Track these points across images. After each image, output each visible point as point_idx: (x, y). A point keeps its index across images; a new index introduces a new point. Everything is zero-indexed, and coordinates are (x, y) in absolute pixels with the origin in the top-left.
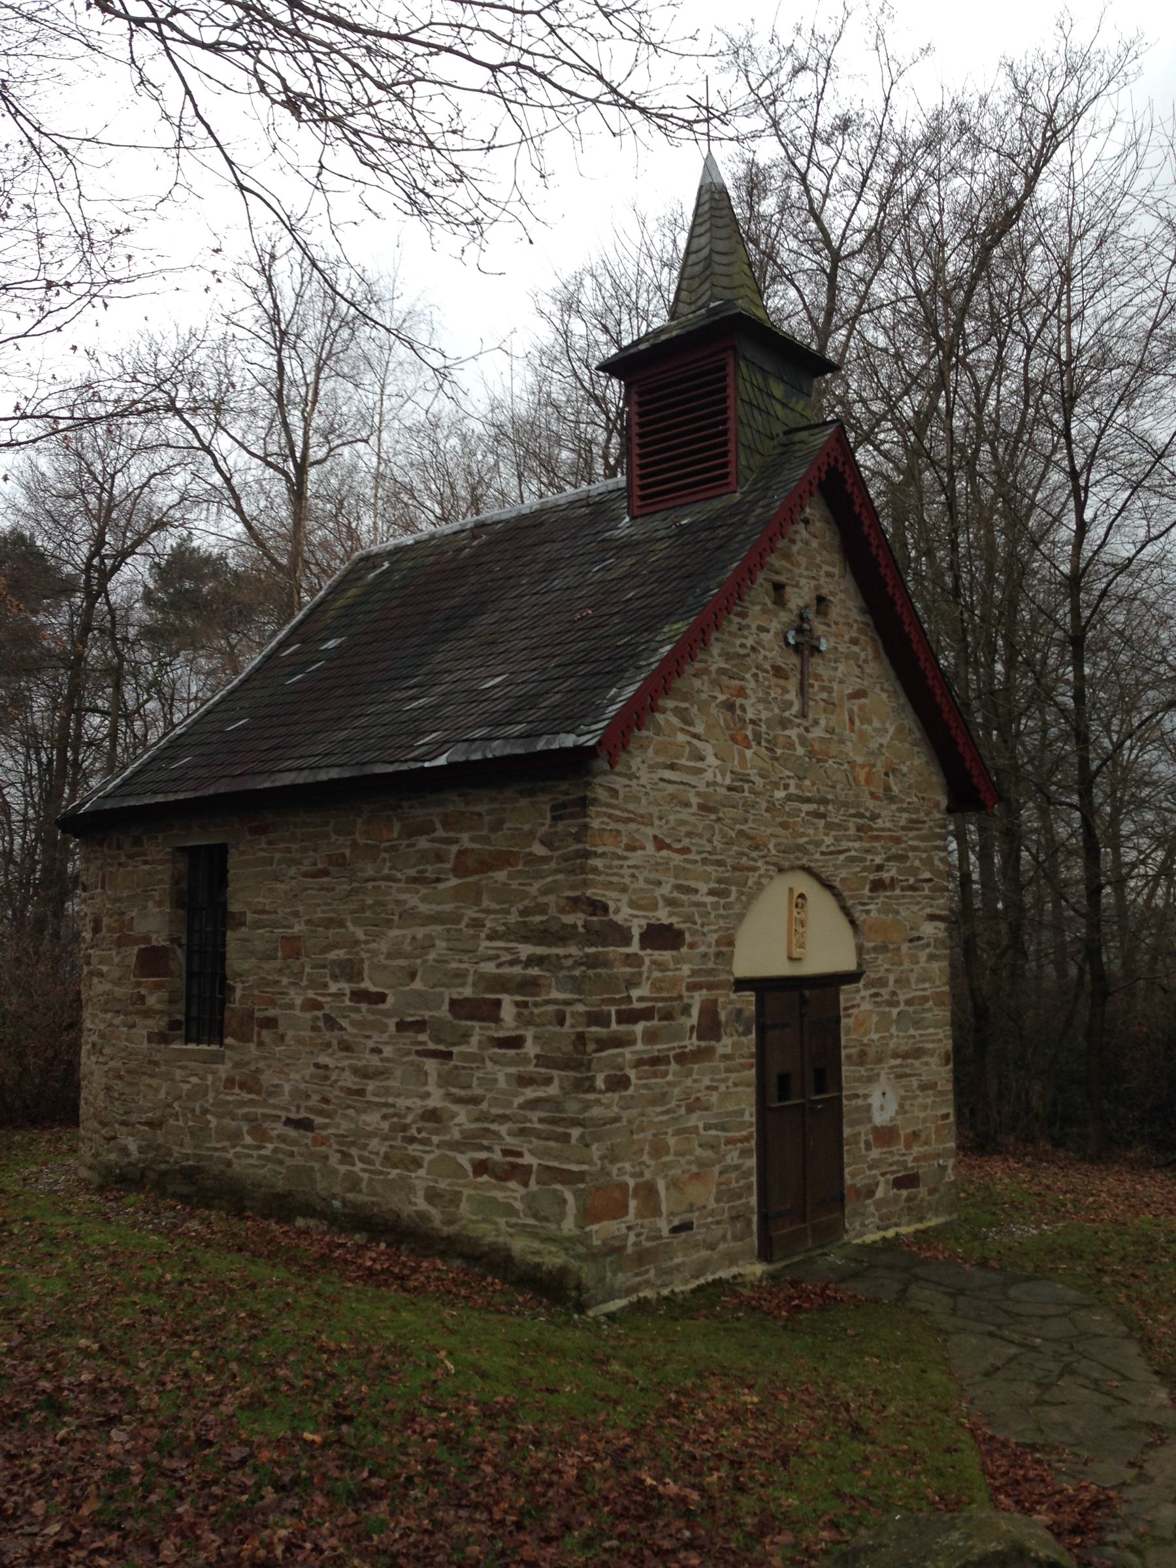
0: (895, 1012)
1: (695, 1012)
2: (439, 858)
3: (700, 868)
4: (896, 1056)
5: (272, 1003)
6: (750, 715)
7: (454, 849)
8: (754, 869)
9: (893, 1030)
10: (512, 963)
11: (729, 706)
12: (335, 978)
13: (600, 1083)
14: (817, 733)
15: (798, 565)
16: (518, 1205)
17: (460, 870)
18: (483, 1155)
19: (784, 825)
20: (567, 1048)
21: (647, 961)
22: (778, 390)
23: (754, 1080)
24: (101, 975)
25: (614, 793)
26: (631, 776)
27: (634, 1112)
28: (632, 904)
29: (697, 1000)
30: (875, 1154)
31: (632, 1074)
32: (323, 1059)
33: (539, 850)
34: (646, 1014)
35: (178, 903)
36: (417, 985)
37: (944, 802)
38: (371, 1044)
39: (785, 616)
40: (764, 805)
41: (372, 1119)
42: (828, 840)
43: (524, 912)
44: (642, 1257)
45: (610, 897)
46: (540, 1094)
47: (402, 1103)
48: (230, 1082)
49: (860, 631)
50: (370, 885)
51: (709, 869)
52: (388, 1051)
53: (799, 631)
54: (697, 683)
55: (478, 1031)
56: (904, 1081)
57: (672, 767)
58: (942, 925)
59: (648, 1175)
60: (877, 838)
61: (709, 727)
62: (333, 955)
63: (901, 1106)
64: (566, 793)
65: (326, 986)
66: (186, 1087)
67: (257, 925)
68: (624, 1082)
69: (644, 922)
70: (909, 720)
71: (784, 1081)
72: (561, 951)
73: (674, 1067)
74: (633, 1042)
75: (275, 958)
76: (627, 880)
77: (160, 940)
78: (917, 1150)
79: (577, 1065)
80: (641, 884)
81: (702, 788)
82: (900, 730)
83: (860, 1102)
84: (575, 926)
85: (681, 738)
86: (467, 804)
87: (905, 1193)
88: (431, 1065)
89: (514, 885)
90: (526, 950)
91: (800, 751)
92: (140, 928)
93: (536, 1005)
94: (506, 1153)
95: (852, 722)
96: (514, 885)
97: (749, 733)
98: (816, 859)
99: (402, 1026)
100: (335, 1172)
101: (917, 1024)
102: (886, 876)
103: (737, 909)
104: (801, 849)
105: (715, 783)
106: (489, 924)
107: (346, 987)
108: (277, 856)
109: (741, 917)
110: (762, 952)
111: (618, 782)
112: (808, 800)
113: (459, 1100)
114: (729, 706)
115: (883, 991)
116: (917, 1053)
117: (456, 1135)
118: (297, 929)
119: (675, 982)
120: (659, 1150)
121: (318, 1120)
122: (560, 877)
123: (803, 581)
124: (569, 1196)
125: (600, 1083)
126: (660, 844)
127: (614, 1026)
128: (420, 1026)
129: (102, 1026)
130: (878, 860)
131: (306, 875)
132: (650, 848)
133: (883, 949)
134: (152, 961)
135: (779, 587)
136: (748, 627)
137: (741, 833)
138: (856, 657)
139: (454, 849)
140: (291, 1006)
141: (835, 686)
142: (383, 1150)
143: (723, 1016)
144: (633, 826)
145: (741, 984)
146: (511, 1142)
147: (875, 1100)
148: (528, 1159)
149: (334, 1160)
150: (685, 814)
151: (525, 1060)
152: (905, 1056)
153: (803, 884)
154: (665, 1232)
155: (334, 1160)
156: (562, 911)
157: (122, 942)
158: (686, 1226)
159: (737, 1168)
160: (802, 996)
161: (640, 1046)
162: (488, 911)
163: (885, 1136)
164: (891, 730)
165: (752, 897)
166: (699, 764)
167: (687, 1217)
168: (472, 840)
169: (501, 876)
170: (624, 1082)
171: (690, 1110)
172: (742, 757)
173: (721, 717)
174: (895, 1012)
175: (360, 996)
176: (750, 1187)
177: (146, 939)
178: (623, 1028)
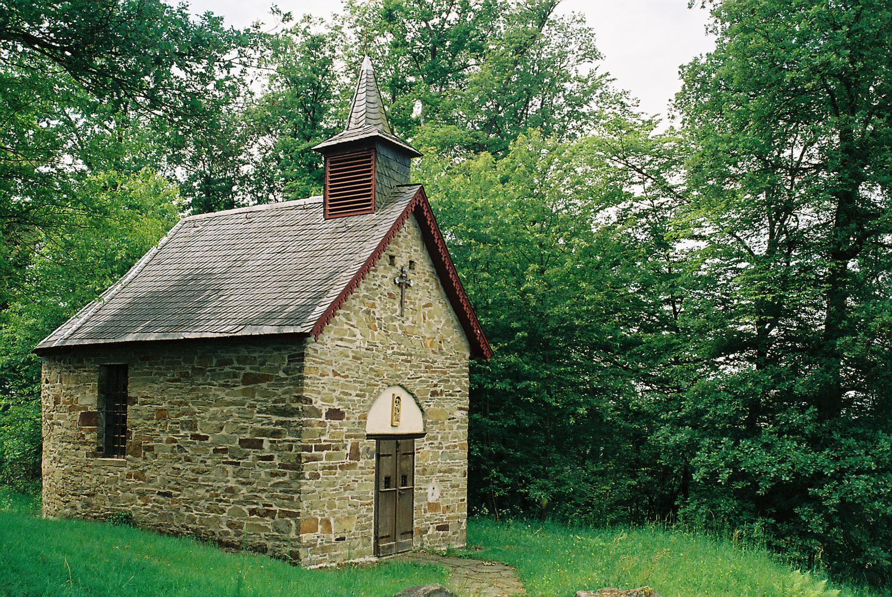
0: (441, 451)
1: (349, 447)
2: (235, 376)
3: (353, 384)
4: (440, 472)
5: (151, 439)
6: (377, 316)
7: (242, 372)
8: (377, 385)
9: (439, 460)
10: (268, 424)
11: (368, 312)
12: (183, 429)
13: (307, 476)
14: (407, 323)
15: (401, 247)
16: (269, 527)
17: (245, 381)
18: (254, 507)
19: (391, 366)
20: (293, 461)
21: (328, 424)
22: (395, 165)
23: (374, 479)
24: (59, 424)
25: (316, 351)
26: (324, 344)
27: (322, 489)
28: (322, 400)
29: (350, 442)
30: (428, 514)
31: (321, 473)
32: (177, 465)
33: (282, 375)
34: (328, 448)
35: (101, 391)
36: (224, 432)
37: (468, 355)
38: (200, 458)
39: (394, 270)
40: (382, 357)
41: (201, 492)
42: (412, 373)
43: (275, 402)
44: (324, 549)
45: (313, 396)
46: (281, 480)
47: (216, 484)
48: (129, 476)
49: (430, 276)
50: (201, 387)
51: (357, 385)
52: (209, 462)
53: (401, 277)
54: (353, 302)
55: (252, 453)
56: (444, 483)
57: (341, 340)
58: (465, 412)
59: (326, 516)
60: (435, 372)
61: (359, 322)
62: (182, 418)
63: (442, 494)
64: (295, 350)
65: (178, 432)
66: (106, 477)
67: (143, 403)
68: (317, 476)
69: (327, 408)
70: (452, 316)
71: (388, 480)
72: (291, 419)
73: (339, 471)
74: (322, 459)
75: (153, 419)
76: (320, 389)
77: (92, 409)
78: (448, 514)
79: (298, 468)
80: (326, 391)
81: (355, 349)
82: (447, 321)
83: (422, 491)
84: (298, 409)
85: (346, 327)
86: (249, 352)
87: (441, 532)
88: (230, 468)
89: (270, 389)
90: (275, 418)
91: (400, 332)
92: (83, 402)
93: (279, 442)
94: (264, 505)
95: (424, 318)
96: (270, 389)
97: (376, 324)
98: (405, 382)
99: (216, 451)
100: (182, 515)
101: (451, 458)
102: (438, 389)
103: (369, 402)
104: (399, 376)
105: (360, 347)
106: (258, 407)
107: (189, 433)
108: (155, 371)
109: (370, 407)
110: (379, 421)
111: (318, 346)
112: (404, 354)
113: (243, 484)
114: (368, 312)
115: (435, 442)
116: (450, 471)
117: (241, 498)
118: (163, 406)
119: (340, 434)
120: (331, 506)
121: (175, 493)
122: (292, 387)
123: (403, 254)
124: (292, 522)
125: (307, 476)
126: (335, 374)
127: (313, 452)
128: (225, 451)
129: (61, 449)
130: (435, 382)
131: (168, 381)
132: (331, 375)
133: (436, 423)
134: (87, 418)
135: (392, 257)
136: (377, 276)
137: (371, 368)
138: (428, 288)
139: (242, 372)
140: (161, 441)
141: (417, 302)
142: (206, 505)
143: (361, 451)
144: (324, 365)
145: (369, 437)
146: (267, 501)
147: (430, 491)
148: (274, 508)
149: (182, 510)
150: (346, 360)
151: (275, 466)
152: (445, 472)
153: (399, 391)
154: (333, 540)
155: (182, 510)
156: (292, 402)
157: (71, 410)
158: (343, 539)
159: (365, 516)
160: (397, 443)
161: (324, 461)
162: (257, 401)
163: (434, 507)
164: (443, 322)
165: (375, 398)
166: (354, 338)
167: (343, 535)
168: (251, 369)
169: (264, 385)
170: (317, 476)
171: (345, 490)
172: (373, 334)
173: (364, 317)
174: (441, 451)
175: (196, 437)
176: (371, 525)
177: (85, 408)
178: (318, 453)
